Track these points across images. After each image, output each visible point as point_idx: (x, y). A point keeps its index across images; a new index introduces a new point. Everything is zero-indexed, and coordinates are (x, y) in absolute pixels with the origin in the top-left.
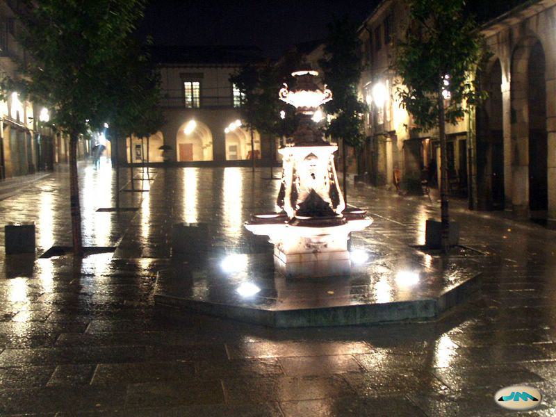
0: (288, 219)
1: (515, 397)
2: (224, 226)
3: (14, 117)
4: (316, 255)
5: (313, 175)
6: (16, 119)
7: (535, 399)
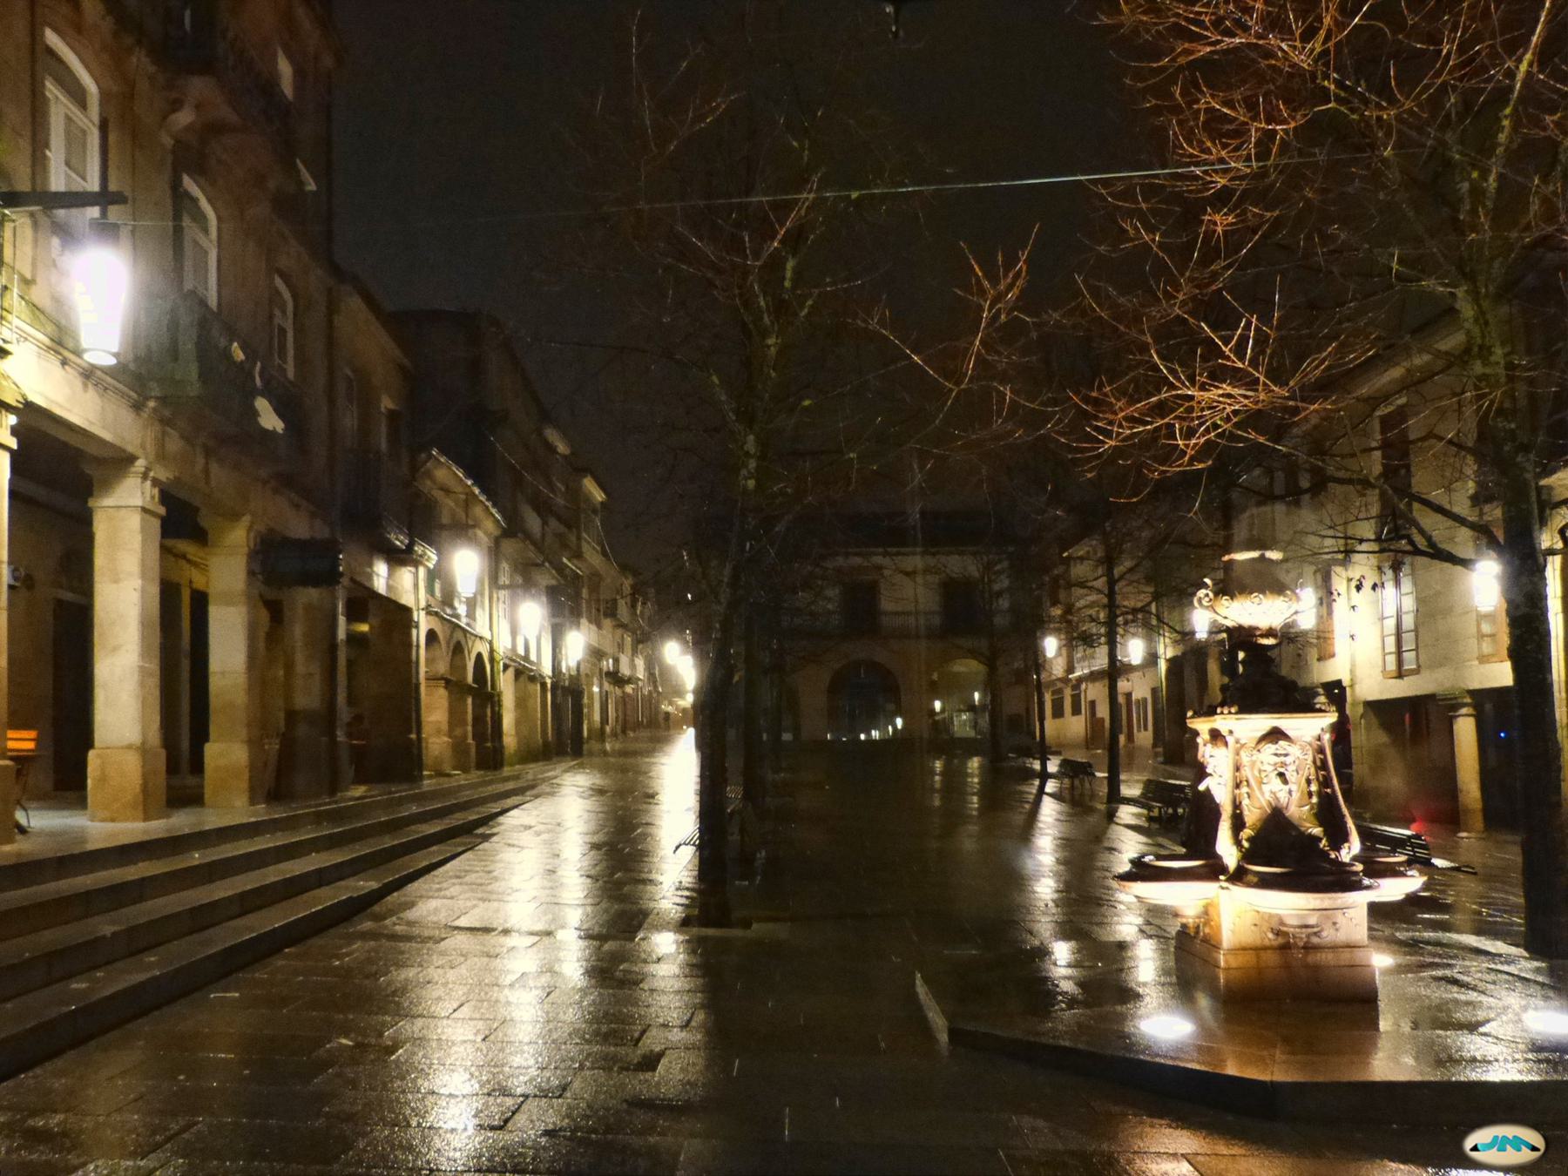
0: (1223, 869)
1: (1500, 1144)
2: (1170, 984)
3: (521, 651)
4: (1307, 954)
5: (1352, 637)
6: (522, 653)
7: (1534, 1149)
